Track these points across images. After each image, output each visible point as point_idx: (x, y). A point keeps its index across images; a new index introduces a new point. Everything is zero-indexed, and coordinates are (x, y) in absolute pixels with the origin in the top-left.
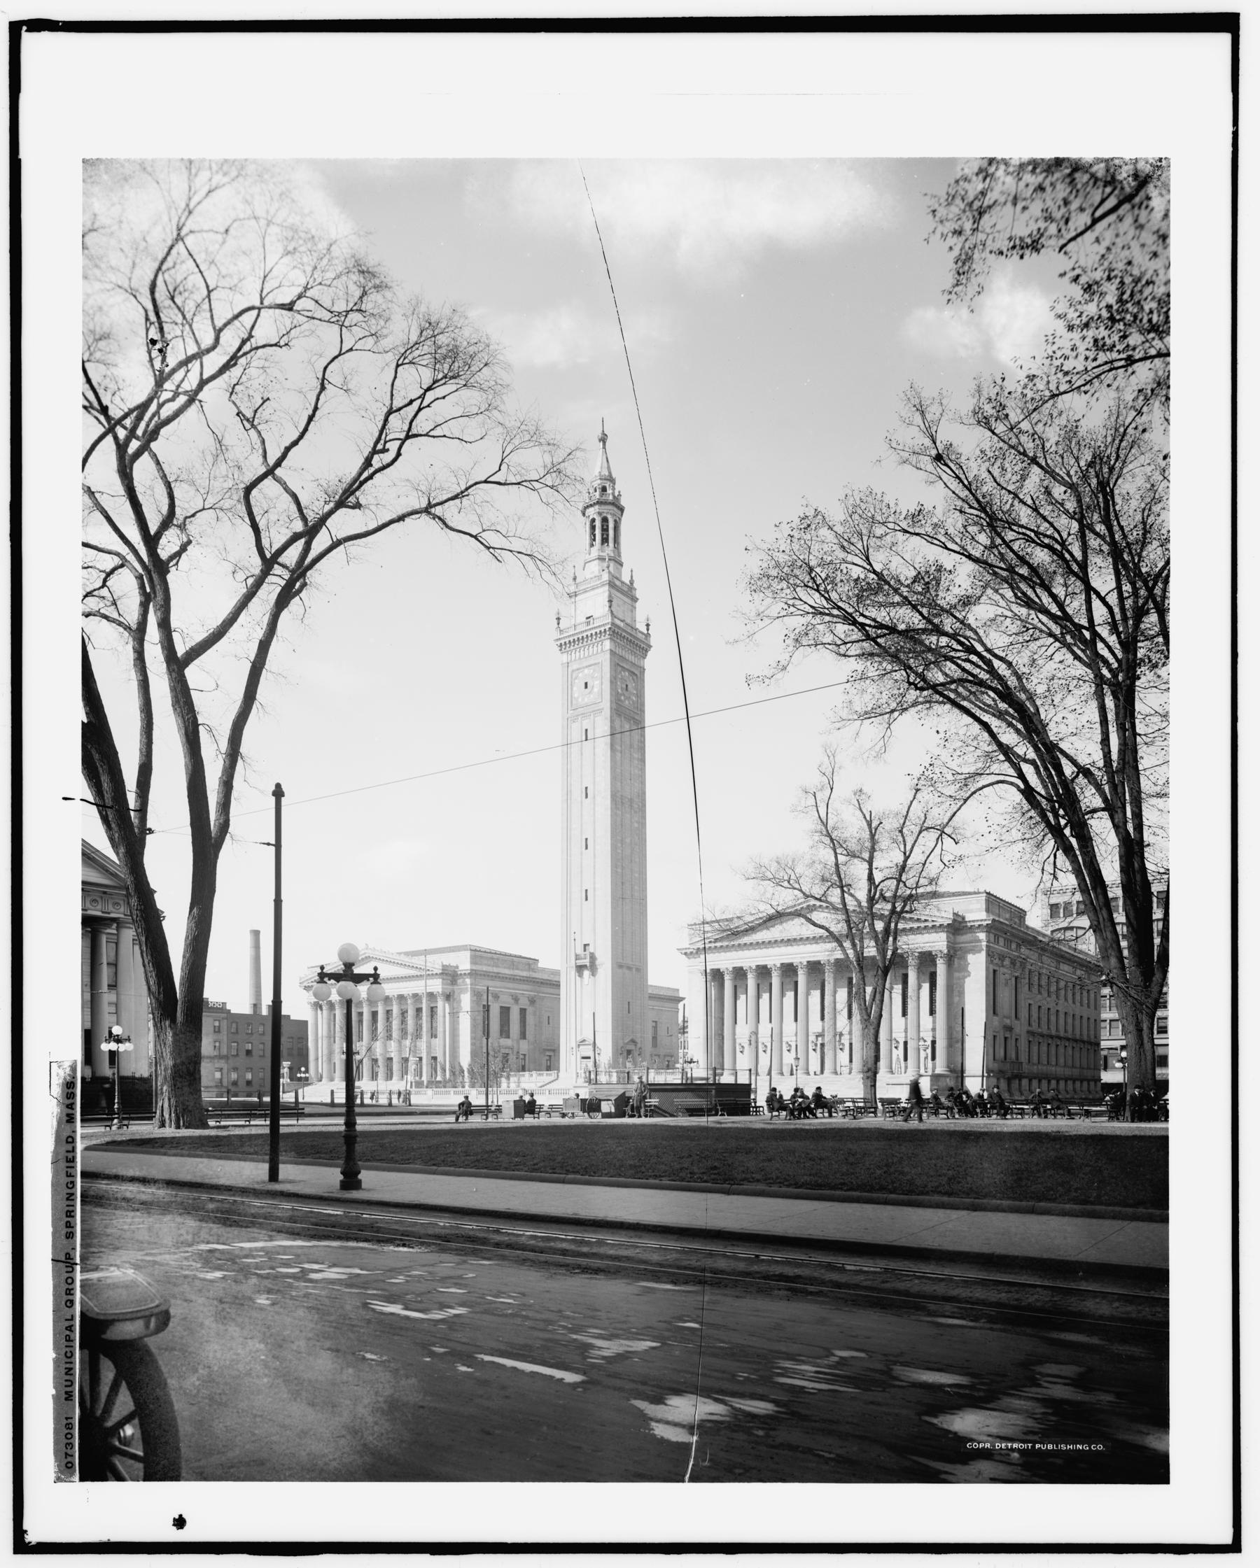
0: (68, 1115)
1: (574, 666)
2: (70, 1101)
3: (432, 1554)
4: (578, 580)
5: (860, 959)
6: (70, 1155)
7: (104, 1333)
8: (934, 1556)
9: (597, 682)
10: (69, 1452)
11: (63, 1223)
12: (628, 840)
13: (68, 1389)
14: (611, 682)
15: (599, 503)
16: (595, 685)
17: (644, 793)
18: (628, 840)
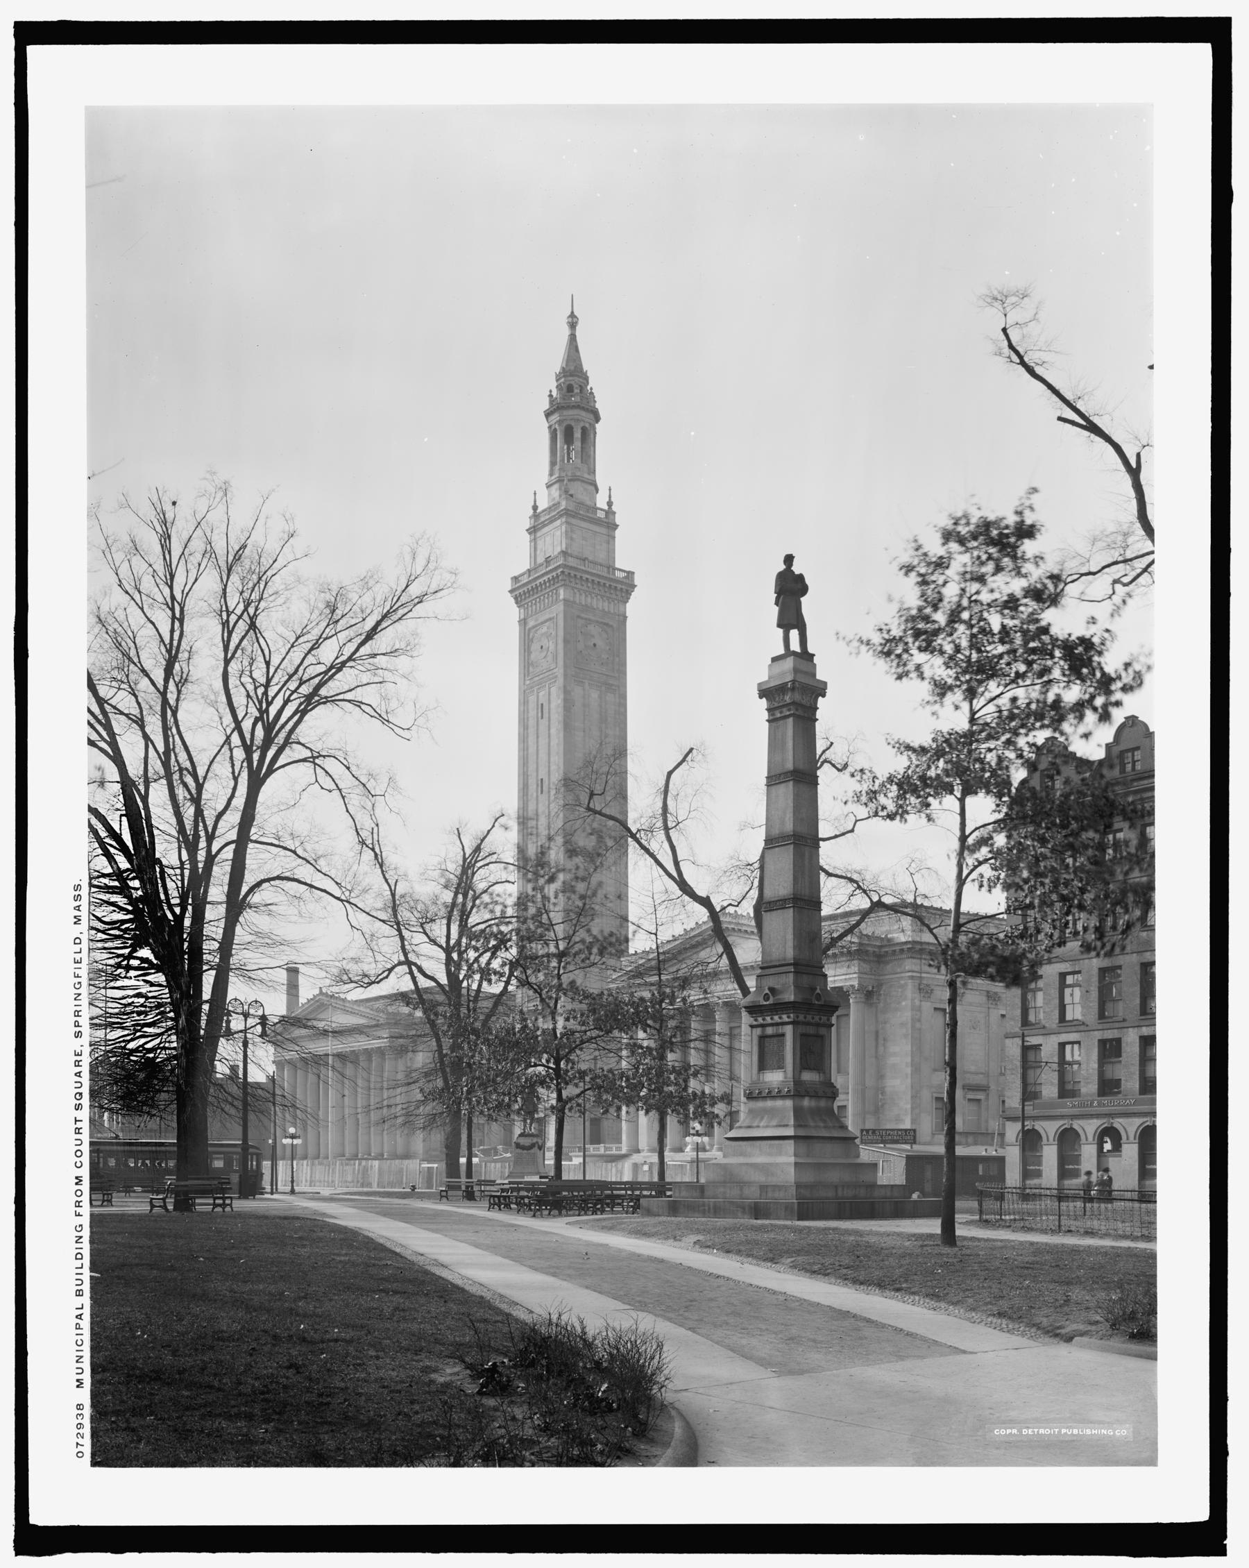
1: (531, 623)
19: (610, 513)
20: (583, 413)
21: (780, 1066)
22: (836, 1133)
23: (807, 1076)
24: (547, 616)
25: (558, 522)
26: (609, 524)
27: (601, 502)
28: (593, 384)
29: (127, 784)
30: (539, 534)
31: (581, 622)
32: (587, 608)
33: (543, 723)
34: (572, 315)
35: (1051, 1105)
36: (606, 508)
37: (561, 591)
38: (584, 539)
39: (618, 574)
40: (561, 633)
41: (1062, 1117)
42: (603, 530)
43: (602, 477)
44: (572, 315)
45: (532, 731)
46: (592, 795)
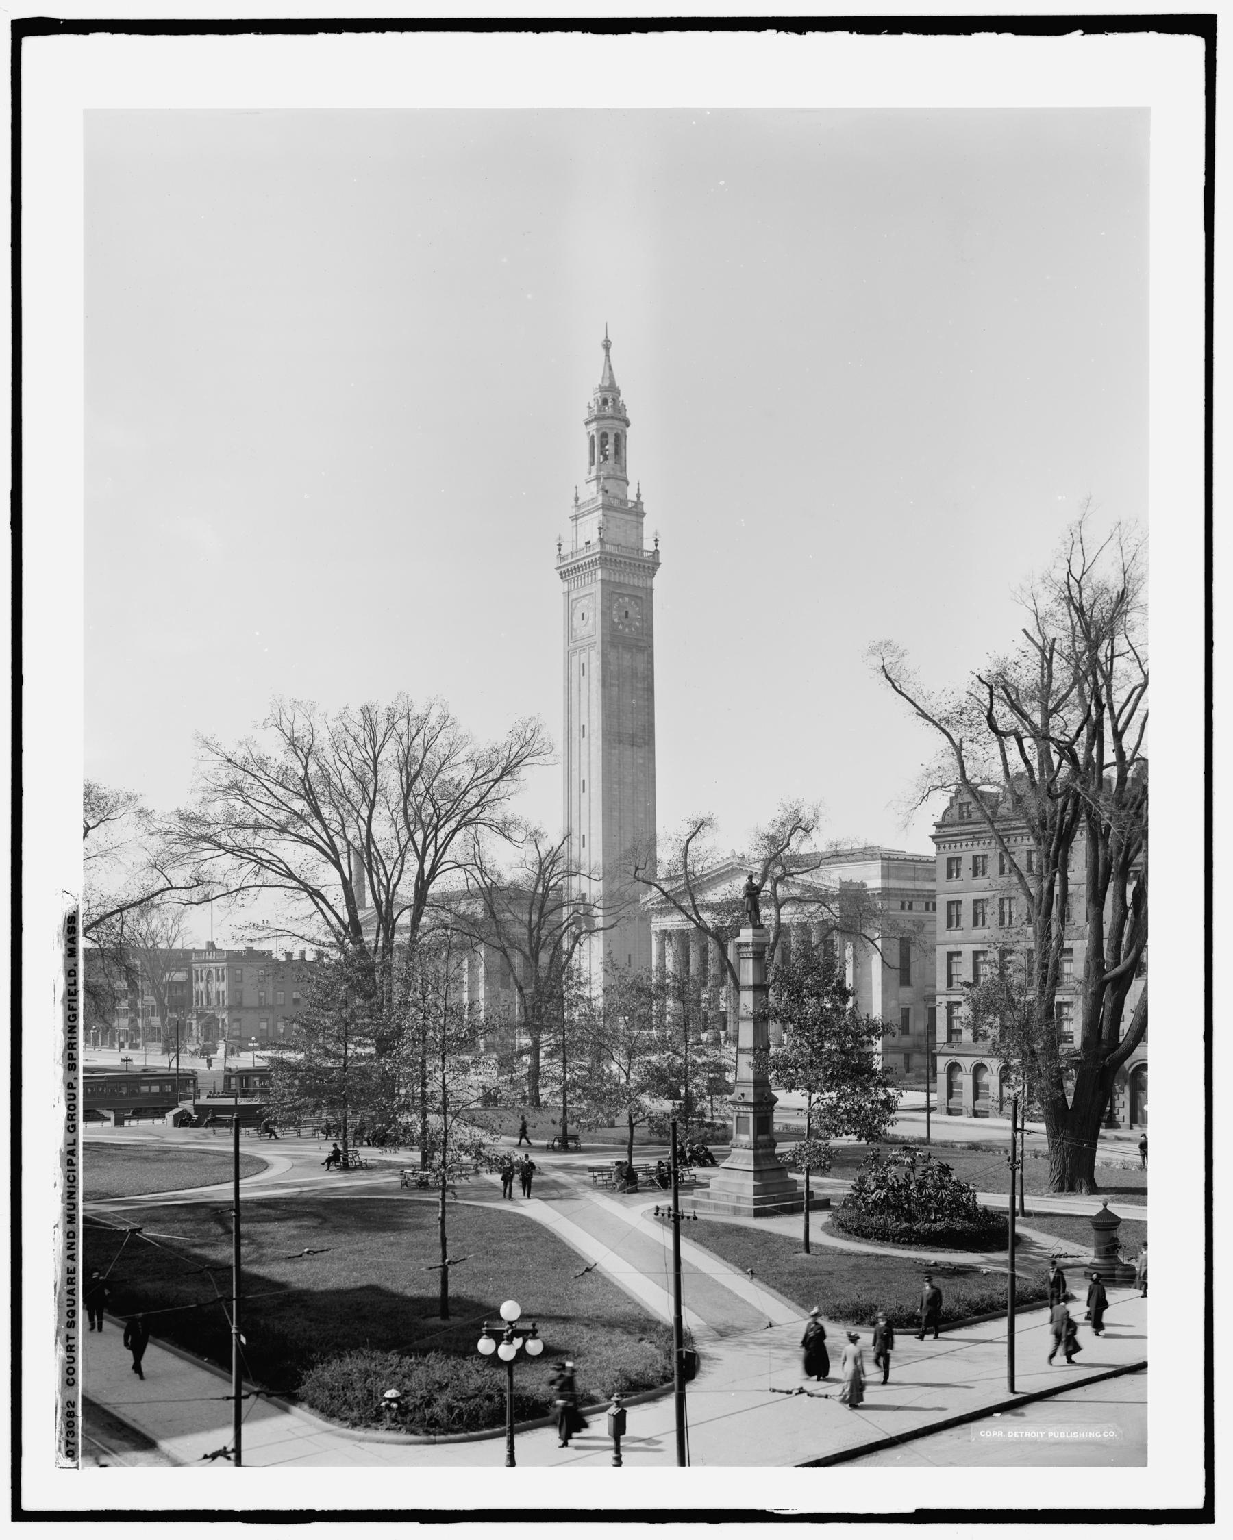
0: (69, 949)
1: (573, 596)
2: (71, 1287)
3: (422, 1522)
4: (580, 502)
5: (702, 929)
6: (72, 989)
7: (109, 1313)
8: (913, 1525)
9: (592, 614)
10: (71, 1440)
11: (64, 1336)
12: (628, 780)
13: (72, 1212)
14: (603, 613)
15: (596, 419)
16: (590, 615)
17: (652, 725)
18: (628, 780)
19: (639, 503)
20: (616, 422)
21: (747, 1132)
22: (776, 1167)
23: (761, 1138)
24: (588, 592)
25: (596, 514)
26: (638, 512)
27: (632, 496)
28: (624, 397)
29: (346, 884)
30: (579, 521)
31: (616, 596)
32: (620, 585)
33: (584, 680)
34: (609, 397)
35: (969, 1047)
36: (635, 499)
37: (599, 572)
38: (618, 527)
39: (645, 554)
40: (599, 607)
41: (976, 1056)
42: (633, 518)
43: (631, 474)
44: (609, 397)
45: (575, 685)
46: (637, 869)
